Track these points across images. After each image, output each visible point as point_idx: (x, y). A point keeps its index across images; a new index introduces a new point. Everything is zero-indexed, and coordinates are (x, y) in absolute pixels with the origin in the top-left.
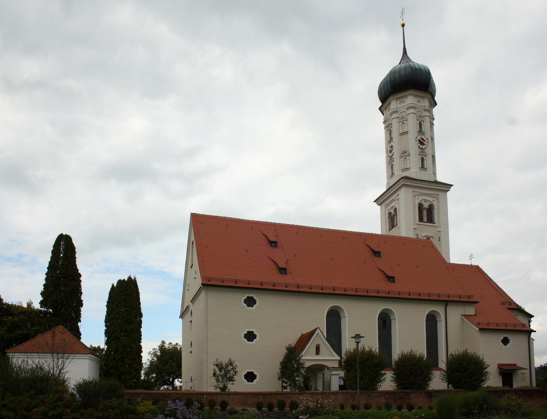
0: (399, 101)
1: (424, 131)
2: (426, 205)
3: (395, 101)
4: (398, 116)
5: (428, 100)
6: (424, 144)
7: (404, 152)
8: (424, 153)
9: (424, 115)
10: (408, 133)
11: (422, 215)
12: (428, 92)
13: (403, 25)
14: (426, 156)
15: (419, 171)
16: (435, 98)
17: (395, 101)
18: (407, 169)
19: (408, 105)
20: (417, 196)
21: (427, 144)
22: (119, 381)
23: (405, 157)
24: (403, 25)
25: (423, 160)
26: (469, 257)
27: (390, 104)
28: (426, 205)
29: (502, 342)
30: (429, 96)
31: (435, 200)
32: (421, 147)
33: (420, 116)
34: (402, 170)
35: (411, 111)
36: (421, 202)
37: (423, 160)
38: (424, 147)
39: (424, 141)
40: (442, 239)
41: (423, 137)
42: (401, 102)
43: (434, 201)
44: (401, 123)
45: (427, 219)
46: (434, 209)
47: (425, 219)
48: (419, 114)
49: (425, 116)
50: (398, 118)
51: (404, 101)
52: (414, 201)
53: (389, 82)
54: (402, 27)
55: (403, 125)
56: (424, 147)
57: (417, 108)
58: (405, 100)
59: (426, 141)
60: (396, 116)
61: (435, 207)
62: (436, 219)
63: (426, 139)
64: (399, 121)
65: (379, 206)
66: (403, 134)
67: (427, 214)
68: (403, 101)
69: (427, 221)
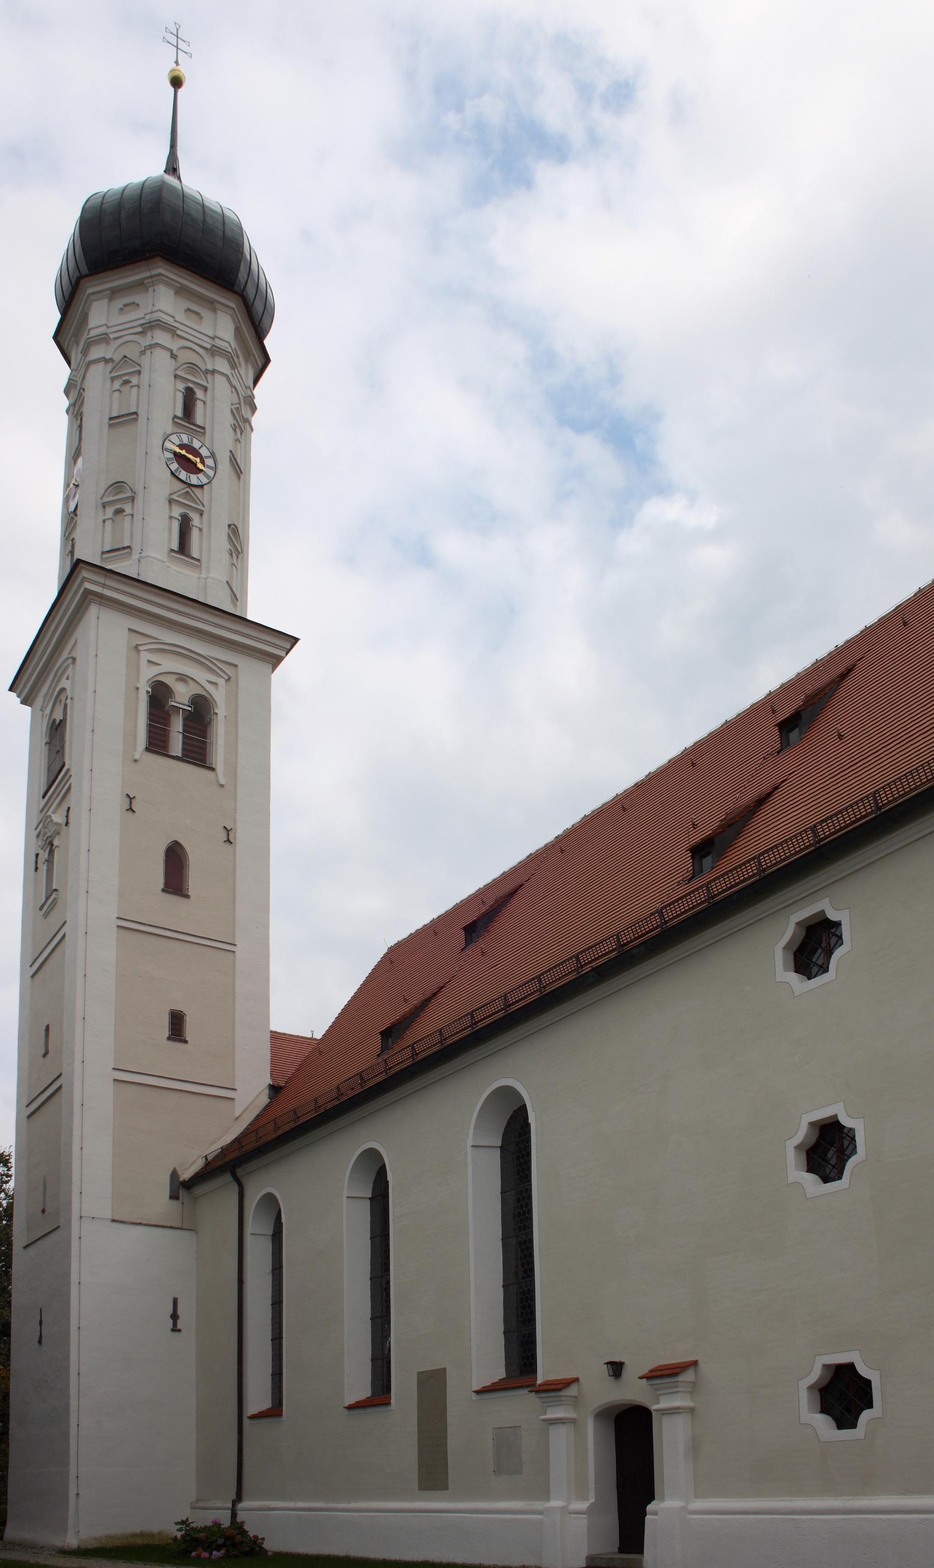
0: (119, 303)
2: (182, 695)
3: (106, 301)
6: (181, 446)
7: (118, 486)
8: (197, 503)
9: (210, 368)
10: (136, 420)
13: (176, 82)
15: (165, 559)
16: (267, 342)
17: (106, 301)
20: (149, 650)
21: (211, 473)
23: (118, 506)
24: (176, 82)
27: (85, 317)
28: (182, 695)
29: (868, 1383)
31: (221, 682)
32: (183, 475)
33: (192, 367)
38: (194, 479)
39: (196, 453)
40: (241, 836)
41: (196, 444)
42: (126, 305)
43: (215, 684)
44: (117, 384)
46: (214, 717)
47: (176, 745)
48: (185, 356)
49: (213, 372)
52: (133, 668)
54: (172, 90)
55: (126, 388)
56: (194, 479)
57: (178, 332)
58: (206, 314)
59: (210, 462)
61: (221, 710)
62: (219, 753)
63: (200, 444)
64: (113, 375)
65: (27, 710)
68: (198, 314)
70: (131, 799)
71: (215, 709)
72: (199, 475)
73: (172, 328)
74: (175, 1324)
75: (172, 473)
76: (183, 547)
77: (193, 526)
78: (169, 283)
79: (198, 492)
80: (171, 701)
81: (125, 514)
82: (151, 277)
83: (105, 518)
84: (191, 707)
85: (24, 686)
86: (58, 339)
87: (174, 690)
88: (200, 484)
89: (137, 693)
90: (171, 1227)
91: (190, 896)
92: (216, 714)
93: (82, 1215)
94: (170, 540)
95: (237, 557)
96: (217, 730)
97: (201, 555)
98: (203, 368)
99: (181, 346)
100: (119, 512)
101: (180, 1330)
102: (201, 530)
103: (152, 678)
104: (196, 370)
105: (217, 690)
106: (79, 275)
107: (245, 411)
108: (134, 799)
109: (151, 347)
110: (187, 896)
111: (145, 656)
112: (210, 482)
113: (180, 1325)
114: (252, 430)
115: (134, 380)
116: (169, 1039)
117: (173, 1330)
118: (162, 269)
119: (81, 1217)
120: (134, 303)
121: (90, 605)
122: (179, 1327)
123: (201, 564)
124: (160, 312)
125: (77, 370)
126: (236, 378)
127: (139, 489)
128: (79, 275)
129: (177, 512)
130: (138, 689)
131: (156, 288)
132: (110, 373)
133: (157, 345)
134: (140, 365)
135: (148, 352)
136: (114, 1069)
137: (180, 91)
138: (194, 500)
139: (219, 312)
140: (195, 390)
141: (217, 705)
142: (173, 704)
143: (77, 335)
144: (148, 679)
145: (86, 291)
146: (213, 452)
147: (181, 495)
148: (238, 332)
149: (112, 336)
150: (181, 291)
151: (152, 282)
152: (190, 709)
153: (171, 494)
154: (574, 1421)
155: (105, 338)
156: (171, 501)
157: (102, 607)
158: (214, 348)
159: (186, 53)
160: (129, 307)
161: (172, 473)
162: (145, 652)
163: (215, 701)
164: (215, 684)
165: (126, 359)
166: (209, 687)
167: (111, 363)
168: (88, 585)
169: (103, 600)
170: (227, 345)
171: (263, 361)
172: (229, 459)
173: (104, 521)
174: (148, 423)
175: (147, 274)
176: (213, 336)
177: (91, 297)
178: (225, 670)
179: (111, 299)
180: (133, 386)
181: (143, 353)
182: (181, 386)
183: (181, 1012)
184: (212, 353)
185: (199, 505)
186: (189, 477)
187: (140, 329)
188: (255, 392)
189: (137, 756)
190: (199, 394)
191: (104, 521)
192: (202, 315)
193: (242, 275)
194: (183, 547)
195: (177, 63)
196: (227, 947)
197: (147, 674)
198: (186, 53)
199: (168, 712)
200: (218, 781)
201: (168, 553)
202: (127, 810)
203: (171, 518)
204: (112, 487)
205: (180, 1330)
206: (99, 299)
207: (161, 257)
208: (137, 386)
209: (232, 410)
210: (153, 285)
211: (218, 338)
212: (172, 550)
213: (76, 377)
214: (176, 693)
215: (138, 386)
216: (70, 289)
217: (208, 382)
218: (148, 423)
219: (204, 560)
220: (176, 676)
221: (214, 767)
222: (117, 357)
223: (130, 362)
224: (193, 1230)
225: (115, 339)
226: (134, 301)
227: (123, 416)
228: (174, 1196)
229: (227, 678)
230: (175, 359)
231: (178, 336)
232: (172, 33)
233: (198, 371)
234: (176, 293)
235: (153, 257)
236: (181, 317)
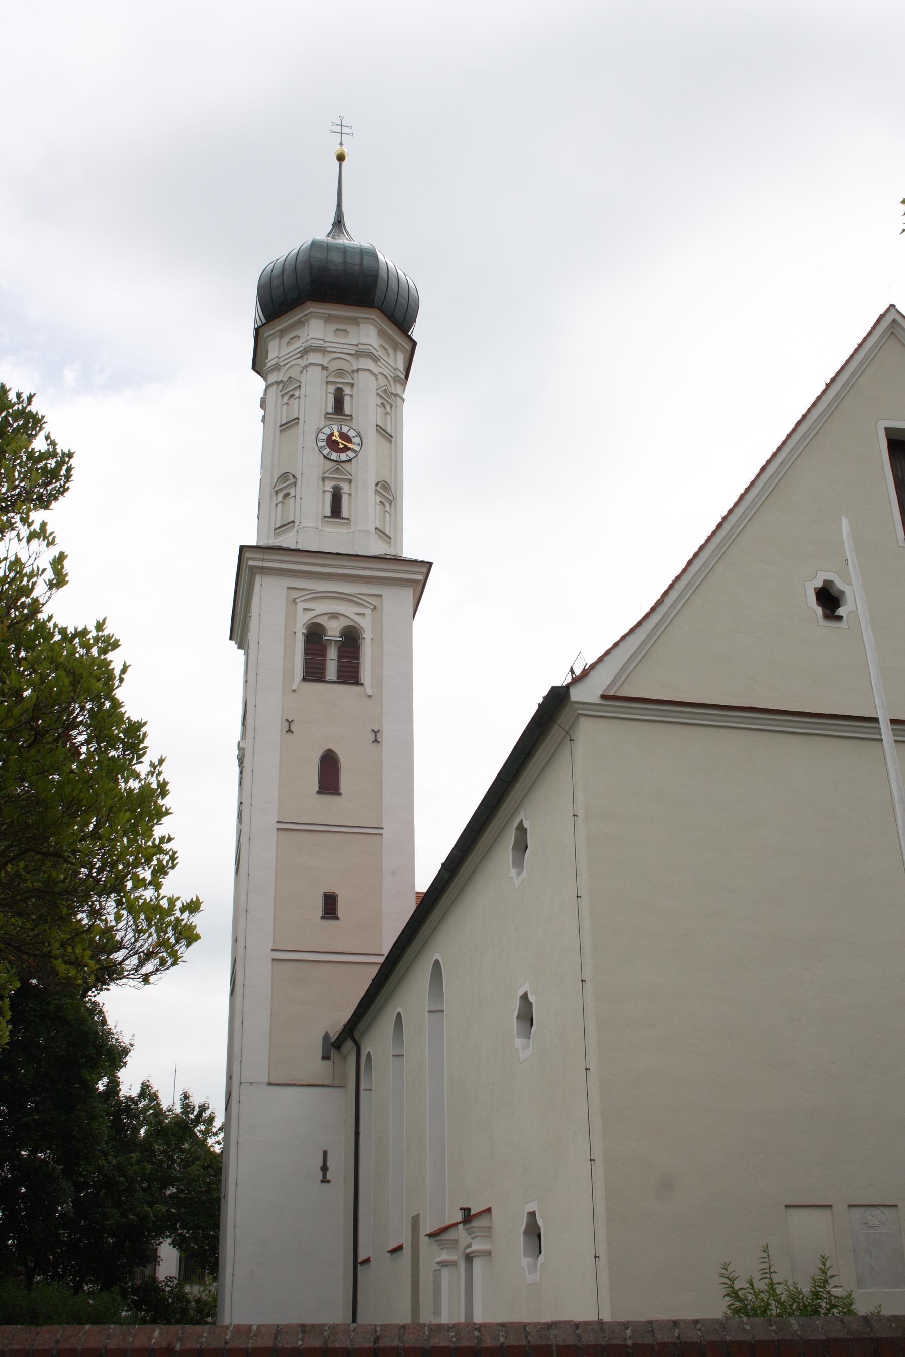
0: (286, 339)
1: (352, 410)
2: (334, 630)
5: (375, 326)
7: (284, 476)
9: (355, 368)
11: (358, 663)
13: (341, 158)
14: (350, 482)
18: (287, 525)
19: (360, 347)
21: (357, 448)
22: (842, 1296)
24: (341, 158)
28: (334, 630)
31: (368, 611)
32: (334, 456)
33: (341, 372)
36: (322, 621)
40: (386, 735)
41: (345, 429)
42: (291, 339)
44: (285, 399)
45: (339, 671)
46: (363, 641)
47: (332, 670)
48: (333, 366)
52: (290, 617)
54: (338, 163)
55: (292, 400)
57: (328, 349)
58: (351, 329)
61: (367, 636)
66: (287, 427)
67: (340, 656)
68: (345, 330)
69: (336, 680)
70: (290, 722)
71: (363, 634)
72: (347, 453)
73: (322, 348)
74: (325, 1175)
75: (325, 456)
76: (336, 511)
77: (343, 493)
78: (318, 316)
79: (347, 466)
80: (325, 636)
81: (290, 496)
82: (305, 315)
83: (277, 502)
84: (342, 637)
85: (237, 636)
87: (327, 627)
88: (349, 459)
89: (295, 636)
90: (323, 1085)
91: (341, 793)
92: (364, 638)
93: (241, 1081)
94: (323, 509)
95: (390, 504)
96: (364, 651)
98: (349, 370)
99: (332, 358)
100: (287, 495)
101: (329, 1181)
102: (350, 494)
103: (307, 622)
104: (343, 373)
105: (364, 619)
108: (292, 722)
109: (306, 367)
110: (340, 794)
111: (301, 606)
112: (357, 455)
113: (329, 1176)
115: (297, 393)
116: (323, 918)
117: (322, 1181)
118: (313, 308)
119: (240, 1083)
120: (296, 336)
121: (255, 577)
122: (328, 1178)
124: (312, 340)
126: (383, 367)
127: (298, 476)
129: (329, 486)
130: (295, 633)
131: (310, 322)
132: (280, 391)
133: (311, 364)
134: (300, 382)
135: (305, 371)
136: (272, 950)
138: (343, 472)
139: (361, 325)
140: (344, 388)
141: (364, 631)
142: (326, 638)
144: (304, 623)
145: (264, 335)
146: (359, 432)
147: (332, 472)
149: (282, 364)
150: (328, 319)
151: (306, 319)
152: (341, 639)
153: (323, 474)
155: (276, 367)
156: (323, 479)
157: (263, 575)
158: (357, 353)
160: (294, 340)
161: (325, 456)
162: (302, 603)
163: (362, 628)
164: (363, 614)
165: (291, 379)
166: (358, 619)
168: (251, 563)
169: (264, 571)
171: (411, 345)
173: (276, 504)
174: (304, 424)
175: (302, 314)
176: (357, 344)
177: (267, 339)
178: (370, 602)
179: (281, 337)
180: (296, 398)
181: (302, 372)
182: (332, 389)
183: (334, 893)
184: (357, 357)
185: (347, 476)
186: (339, 456)
187: (299, 355)
189: (294, 687)
190: (347, 390)
191: (276, 504)
194: (336, 511)
195: (341, 144)
196: (375, 831)
197: (302, 620)
199: (325, 644)
200: (366, 693)
201: (322, 520)
202: (287, 732)
203: (324, 491)
204: (280, 479)
205: (329, 1181)
206: (274, 339)
207: (310, 300)
208: (298, 397)
210: (307, 321)
211: (360, 344)
212: (326, 517)
214: (328, 629)
215: (299, 397)
217: (353, 380)
218: (304, 424)
219: (353, 519)
220: (328, 616)
221: (362, 682)
222: (285, 380)
223: (294, 380)
224: (343, 1086)
225: (284, 365)
226: (295, 335)
227: (289, 422)
228: (326, 1057)
229: (372, 607)
230: (327, 370)
231: (329, 352)
232: (337, 125)
233: (345, 374)
234: (326, 321)
235: (303, 302)
236: (330, 337)
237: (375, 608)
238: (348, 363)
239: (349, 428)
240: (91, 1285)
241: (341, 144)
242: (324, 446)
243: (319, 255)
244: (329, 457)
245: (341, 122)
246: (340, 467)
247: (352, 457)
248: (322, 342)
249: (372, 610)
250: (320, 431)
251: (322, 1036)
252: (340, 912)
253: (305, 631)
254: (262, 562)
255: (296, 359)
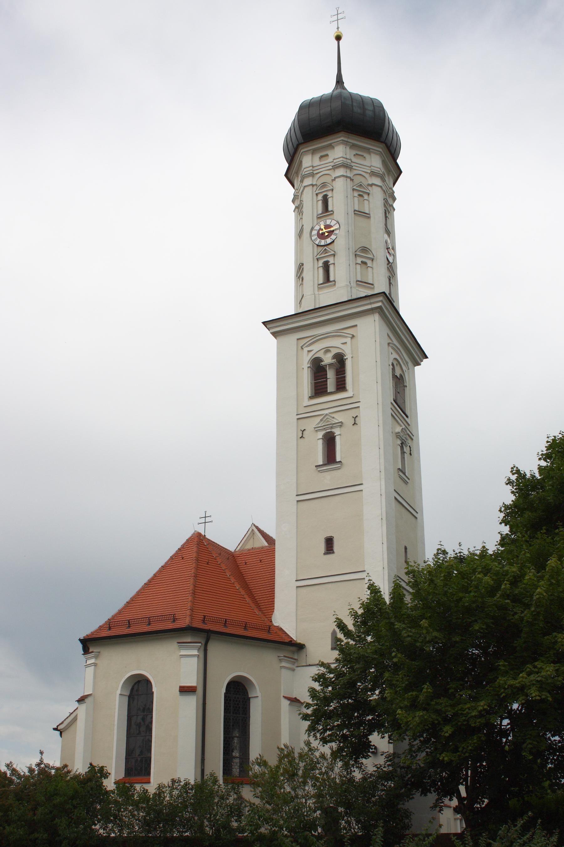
1: (333, 208)
2: (328, 359)
4: (314, 183)
12: (382, 142)
13: (338, 38)
16: (399, 161)
24: (338, 38)
25: (326, 267)
26: (201, 518)
27: (301, 163)
28: (328, 359)
30: (380, 150)
31: (348, 340)
33: (324, 185)
34: (319, 285)
35: (341, 172)
37: (326, 267)
49: (372, 185)
50: (315, 187)
51: (366, 157)
53: (298, 126)
54: (336, 42)
58: (330, 152)
60: (311, 183)
68: (362, 156)
75: (317, 245)
86: (289, 176)
88: (332, 240)
97: (373, 281)
106: (298, 143)
107: (390, 202)
114: (394, 210)
118: (341, 137)
123: (374, 287)
125: (298, 190)
128: (298, 143)
130: (303, 368)
137: (340, 42)
139: (335, 148)
143: (297, 173)
148: (384, 162)
154: (340, 424)
159: (342, 18)
167: (315, 186)
170: (379, 170)
172: (383, 205)
179: (313, 154)
181: (334, 180)
188: (394, 189)
192: (364, 156)
193: (384, 135)
198: (342, 18)
203: (357, 264)
209: (388, 267)
213: (298, 193)
215: (332, 197)
216: (293, 150)
229: (351, 336)
234: (350, 148)
237: (353, 336)
238: (329, 175)
239: (331, 220)
240: (224, 792)
241: (338, 28)
242: (317, 238)
243: (314, 113)
244: (320, 244)
245: (340, 13)
246: (327, 248)
247: (334, 239)
248: (350, 161)
249: (352, 338)
250: (312, 229)
251: (331, 632)
252: (336, 548)
253: (309, 365)
254: (370, 305)
255: (362, 171)
